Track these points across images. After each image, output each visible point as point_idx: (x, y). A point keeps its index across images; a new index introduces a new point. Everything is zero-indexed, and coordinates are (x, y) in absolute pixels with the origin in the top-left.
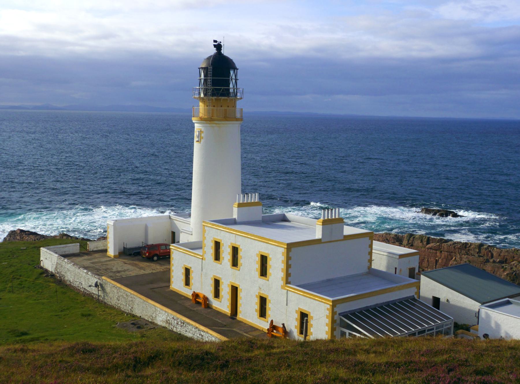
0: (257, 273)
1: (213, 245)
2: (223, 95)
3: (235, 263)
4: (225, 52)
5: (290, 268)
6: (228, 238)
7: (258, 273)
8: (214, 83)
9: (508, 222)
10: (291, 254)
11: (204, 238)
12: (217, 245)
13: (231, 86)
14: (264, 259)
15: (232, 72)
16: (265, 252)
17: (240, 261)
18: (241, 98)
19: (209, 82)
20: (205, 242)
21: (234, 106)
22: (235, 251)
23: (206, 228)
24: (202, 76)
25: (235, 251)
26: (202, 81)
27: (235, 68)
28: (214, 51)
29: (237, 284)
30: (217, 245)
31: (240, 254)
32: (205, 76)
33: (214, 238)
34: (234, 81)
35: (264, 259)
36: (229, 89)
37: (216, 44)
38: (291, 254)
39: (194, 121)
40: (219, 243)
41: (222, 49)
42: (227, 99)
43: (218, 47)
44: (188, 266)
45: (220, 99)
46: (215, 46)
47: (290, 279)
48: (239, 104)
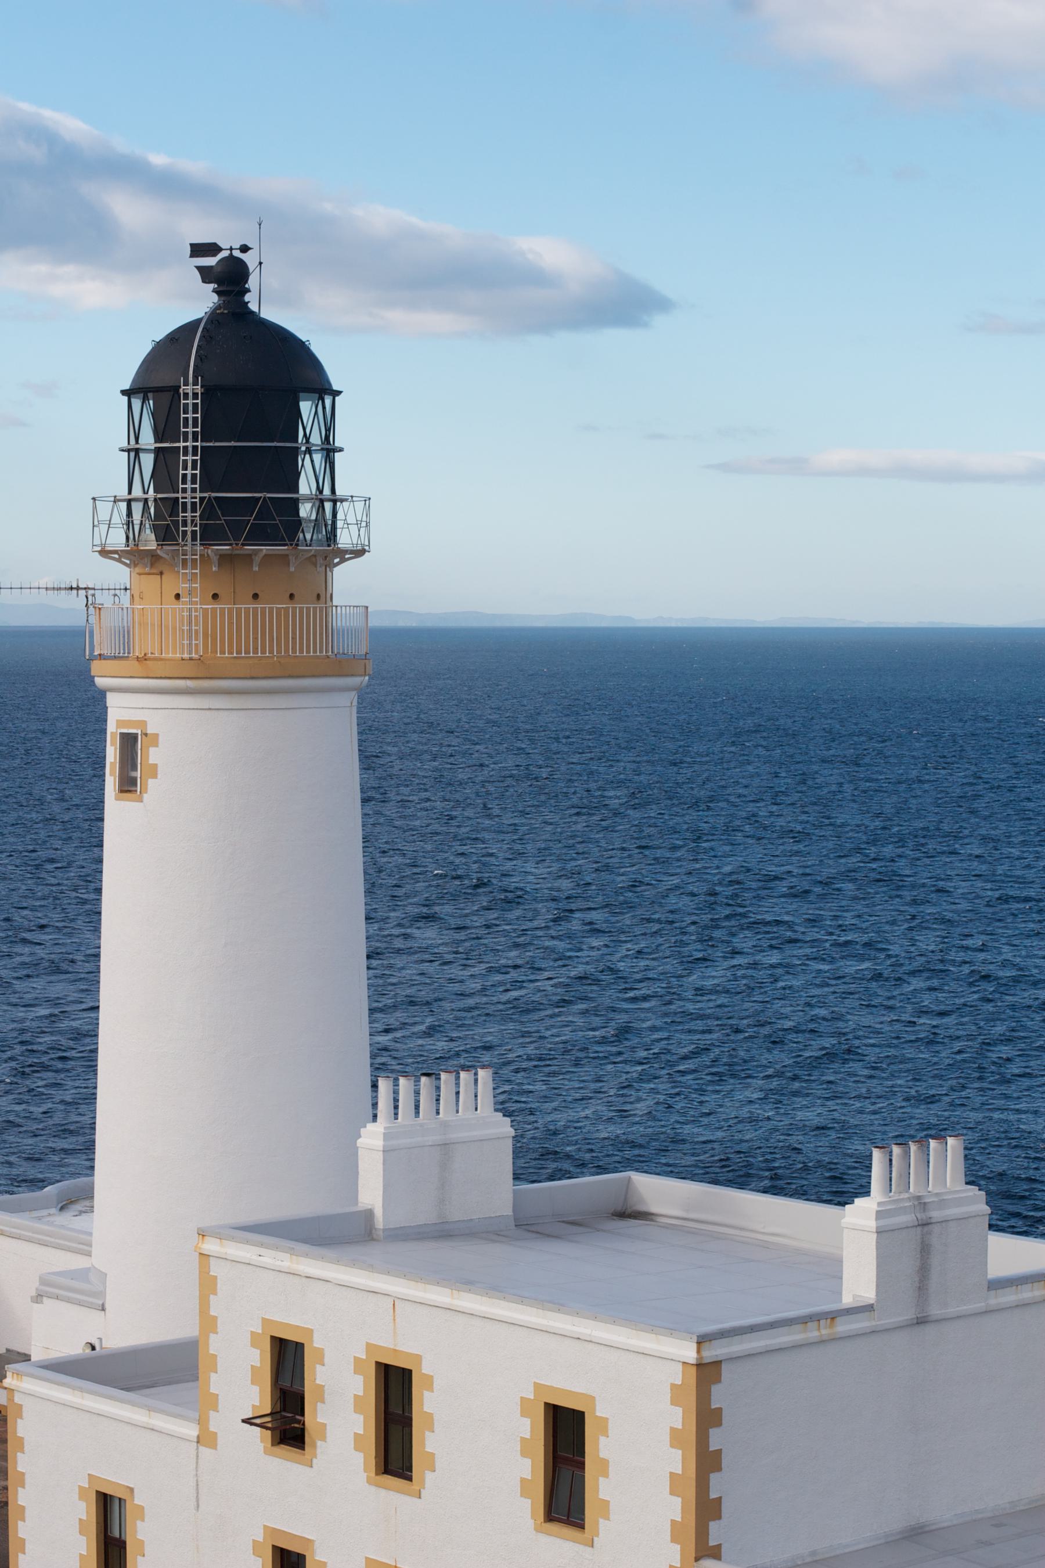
0: (527, 1503)
1: (260, 1358)
2: (261, 534)
3: (395, 1450)
4: (271, 302)
5: (719, 1423)
6: (352, 1317)
7: (525, 1509)
8: (215, 470)
9: (1029, 970)
10: (716, 1439)
11: (209, 1323)
12: (287, 1357)
13: (306, 486)
14: (565, 1434)
15: (306, 407)
16: (570, 1386)
17: (429, 1442)
18: (360, 553)
19: (189, 466)
20: (215, 1344)
21: (322, 596)
22: (395, 1389)
23: (216, 1269)
24: (148, 438)
25: (395, 1389)
26: (148, 461)
27: (322, 389)
28: (199, 302)
29: (282, 1465)
30: (287, 1357)
31: (427, 1402)
32: (159, 437)
33: (265, 1322)
34: (318, 457)
35: (565, 1434)
36: (295, 504)
37: (210, 261)
38: (716, 1439)
39: (100, 682)
40: (299, 1347)
41: (252, 283)
42: (284, 558)
43: (230, 277)
44: (115, 1477)
45: (249, 558)
46: (206, 274)
47: (716, 1532)
48: (346, 582)
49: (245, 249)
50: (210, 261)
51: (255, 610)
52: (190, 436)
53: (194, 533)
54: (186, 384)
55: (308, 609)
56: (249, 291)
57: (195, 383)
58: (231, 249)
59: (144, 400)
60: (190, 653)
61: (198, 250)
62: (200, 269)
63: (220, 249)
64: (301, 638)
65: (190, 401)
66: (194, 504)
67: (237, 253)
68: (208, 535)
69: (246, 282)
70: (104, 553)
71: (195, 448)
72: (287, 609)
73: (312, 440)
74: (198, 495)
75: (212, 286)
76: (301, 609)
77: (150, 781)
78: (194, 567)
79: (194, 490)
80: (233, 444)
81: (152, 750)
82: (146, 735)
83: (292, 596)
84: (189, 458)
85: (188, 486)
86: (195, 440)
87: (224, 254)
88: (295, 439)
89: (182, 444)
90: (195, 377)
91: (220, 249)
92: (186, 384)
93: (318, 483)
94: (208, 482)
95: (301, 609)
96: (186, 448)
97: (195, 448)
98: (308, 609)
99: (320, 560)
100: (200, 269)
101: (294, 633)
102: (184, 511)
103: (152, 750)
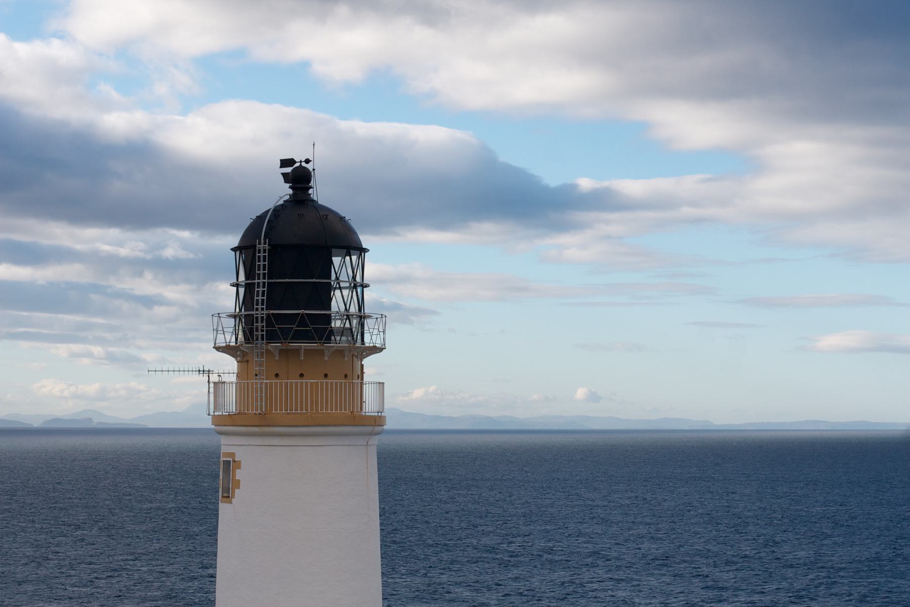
4: (322, 193)
15: (336, 260)
18: (380, 350)
24: (242, 277)
32: (247, 278)
36: (328, 319)
45: (297, 351)
49: (307, 161)
50: (288, 170)
51: (302, 383)
52: (261, 276)
53: (262, 335)
54: (260, 244)
55: (336, 383)
56: (311, 187)
57: (265, 244)
58: (301, 162)
59: (241, 253)
60: (257, 410)
61: (285, 163)
62: (283, 174)
63: (295, 162)
64: (332, 402)
65: (262, 254)
66: (262, 318)
67: (304, 164)
68: (271, 337)
69: (310, 182)
70: (218, 349)
71: (264, 283)
72: (341, 383)
73: (341, 278)
74: (265, 312)
75: (288, 185)
76: (332, 383)
77: (237, 491)
78: (262, 357)
79: (262, 309)
80: (287, 280)
81: (238, 471)
82: (235, 461)
83: (326, 375)
84: (261, 289)
85: (260, 307)
86: (264, 278)
87: (297, 165)
88: (330, 278)
89: (256, 281)
90: (265, 240)
91: (295, 162)
92: (260, 244)
93: (345, 305)
94: (271, 304)
95: (332, 383)
96: (259, 283)
97: (264, 283)
98: (336, 383)
99: (346, 353)
100: (283, 174)
101: (327, 398)
102: (257, 322)
103: (238, 471)
